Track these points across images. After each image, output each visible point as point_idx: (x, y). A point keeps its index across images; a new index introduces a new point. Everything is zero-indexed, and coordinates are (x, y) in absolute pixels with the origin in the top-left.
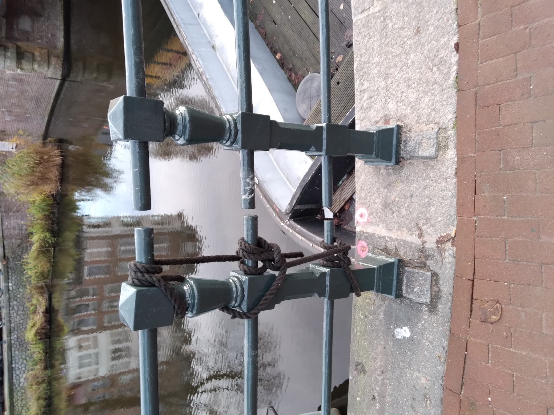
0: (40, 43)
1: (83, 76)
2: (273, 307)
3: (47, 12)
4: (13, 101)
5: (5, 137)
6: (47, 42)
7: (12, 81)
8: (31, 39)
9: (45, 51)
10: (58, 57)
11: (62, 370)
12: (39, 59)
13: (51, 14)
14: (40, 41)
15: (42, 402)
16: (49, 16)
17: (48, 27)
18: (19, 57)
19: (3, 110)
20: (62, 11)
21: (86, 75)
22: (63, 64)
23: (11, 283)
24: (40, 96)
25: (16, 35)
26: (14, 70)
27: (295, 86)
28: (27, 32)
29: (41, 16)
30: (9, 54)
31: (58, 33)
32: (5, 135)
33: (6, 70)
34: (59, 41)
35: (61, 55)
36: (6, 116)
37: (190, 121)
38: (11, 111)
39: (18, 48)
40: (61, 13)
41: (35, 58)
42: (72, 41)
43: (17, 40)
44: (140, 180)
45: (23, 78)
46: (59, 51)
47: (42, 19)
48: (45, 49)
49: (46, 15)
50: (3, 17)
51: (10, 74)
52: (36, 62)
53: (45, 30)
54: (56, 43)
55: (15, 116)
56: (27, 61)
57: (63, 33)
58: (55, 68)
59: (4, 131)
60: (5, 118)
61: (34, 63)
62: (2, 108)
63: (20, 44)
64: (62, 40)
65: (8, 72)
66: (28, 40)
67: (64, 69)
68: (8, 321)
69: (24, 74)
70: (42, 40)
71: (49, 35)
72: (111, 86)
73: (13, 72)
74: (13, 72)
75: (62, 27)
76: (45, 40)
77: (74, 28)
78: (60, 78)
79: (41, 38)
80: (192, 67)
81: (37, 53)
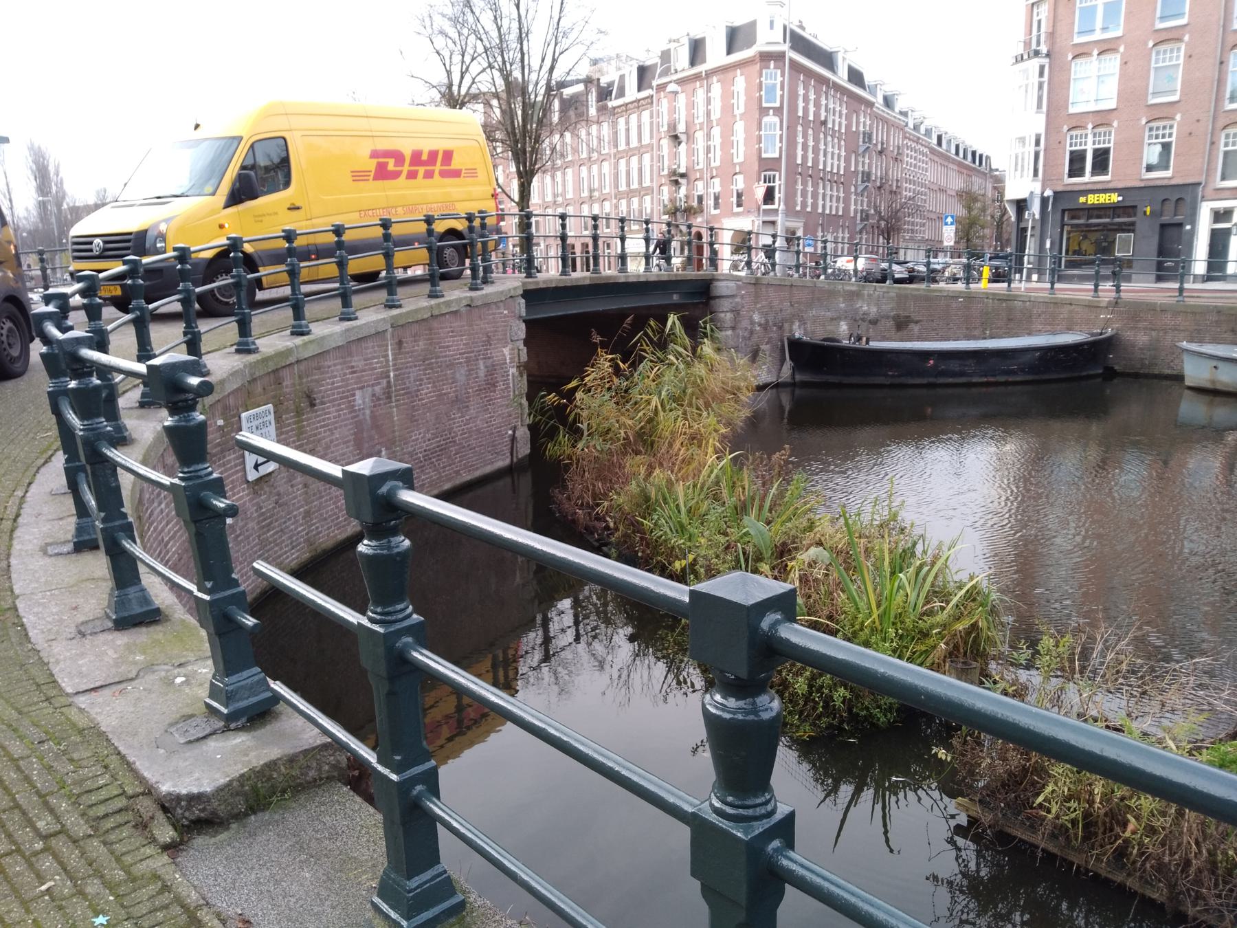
2: (694, 874)
4: (427, 390)
5: (289, 418)
7: (486, 367)
19: (392, 374)
23: (752, 323)
32: (299, 413)
33: (510, 346)
36: (370, 389)
37: (789, 412)
38: (389, 397)
44: (488, 733)
45: (501, 386)
51: (504, 355)
55: (373, 417)
59: (312, 405)
60: (362, 388)
62: (395, 370)
65: (506, 351)
68: (214, 813)
69: (508, 384)
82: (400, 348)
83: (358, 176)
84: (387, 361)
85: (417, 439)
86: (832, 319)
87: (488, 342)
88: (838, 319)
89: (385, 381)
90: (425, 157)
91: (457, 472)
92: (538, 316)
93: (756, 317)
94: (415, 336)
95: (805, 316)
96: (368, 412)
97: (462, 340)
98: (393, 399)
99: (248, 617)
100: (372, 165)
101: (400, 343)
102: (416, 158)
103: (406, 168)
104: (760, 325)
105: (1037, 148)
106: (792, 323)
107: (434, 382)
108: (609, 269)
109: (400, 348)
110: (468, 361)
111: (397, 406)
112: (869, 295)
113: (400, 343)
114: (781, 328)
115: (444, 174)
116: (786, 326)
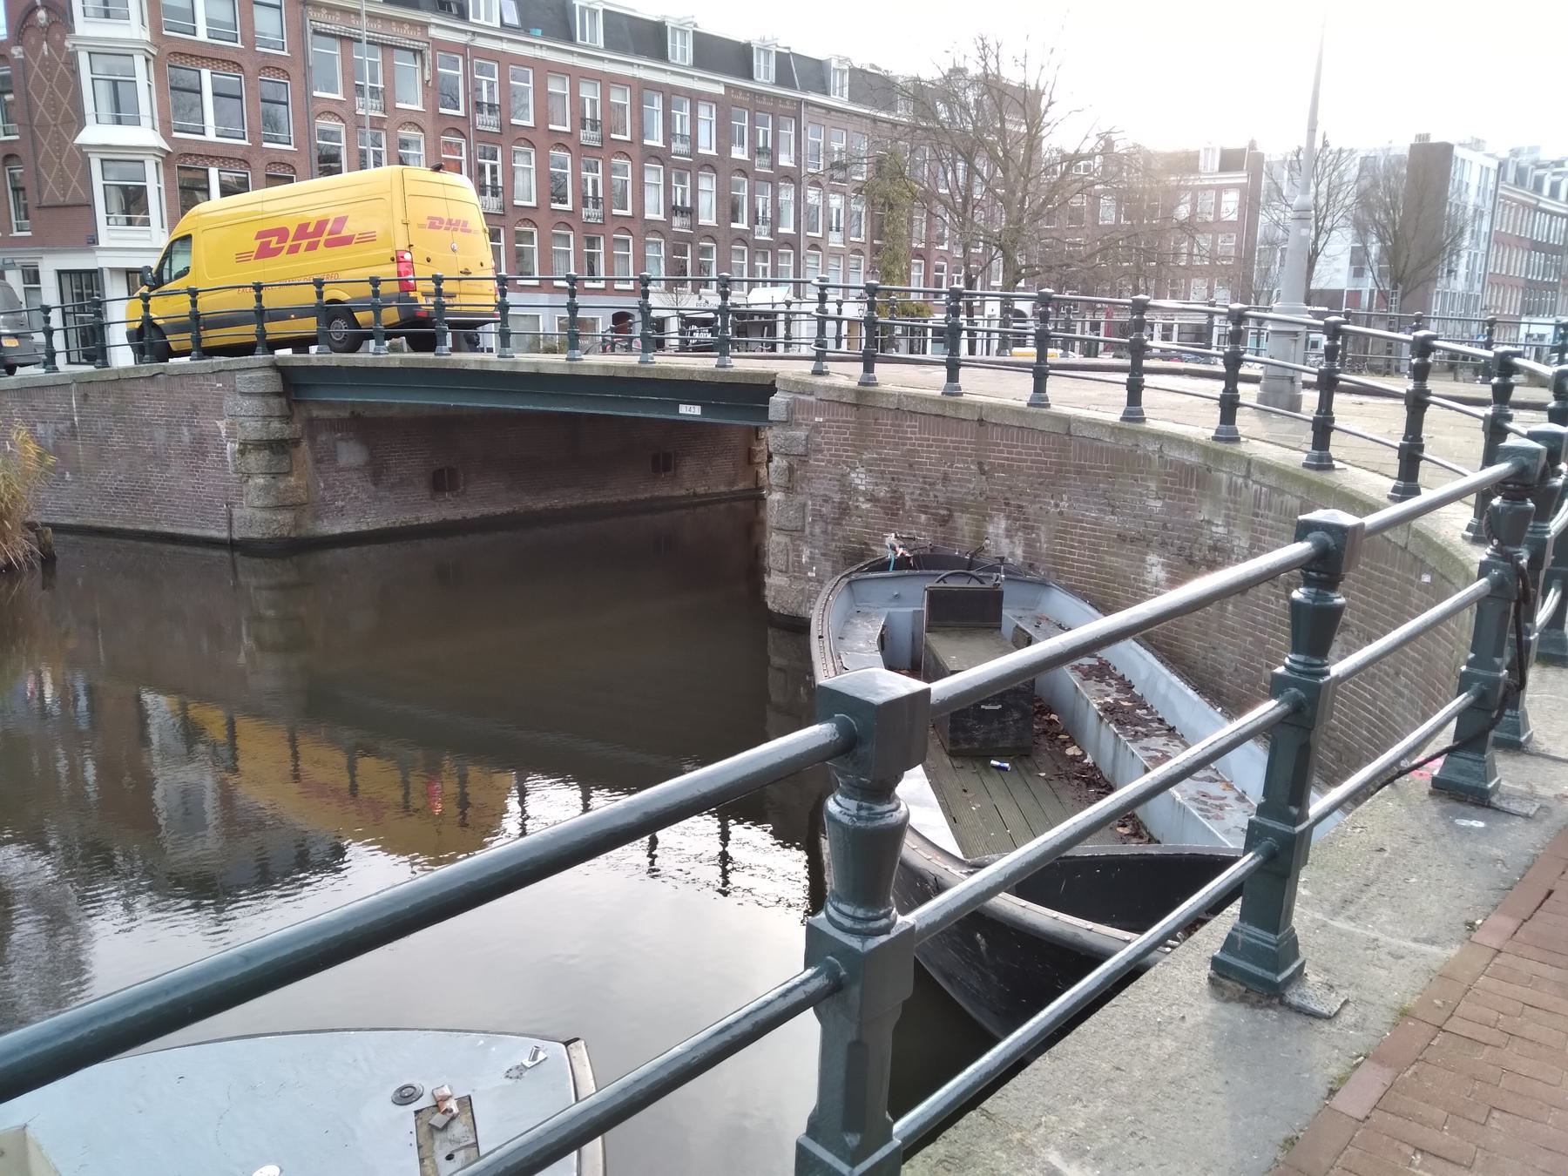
0: (319, 486)
1: (258, 588)
3: (388, 493)
6: (323, 499)
8: (322, 467)
9: (304, 497)
10: (297, 526)
11: (86, 951)
12: (282, 485)
13: (385, 504)
14: (322, 485)
15: (141, 902)
16: (381, 500)
17: (357, 498)
18: (274, 445)
19: (76, 419)
20: (397, 525)
21: (265, 593)
22: (281, 538)
23: (847, 489)
24: (151, 499)
25: (322, 438)
26: (231, 435)
27: (25, 1126)
28: (333, 457)
29: (376, 485)
30: (275, 425)
31: (351, 521)
34: (332, 525)
35: (303, 532)
36: (53, 426)
39: (296, 443)
40: (394, 523)
41: (281, 477)
42: (339, 551)
43: (312, 439)
45: (213, 456)
46: (309, 527)
47: (373, 488)
48: (308, 497)
49: (381, 494)
50: (353, 413)
52: (273, 481)
53: (348, 494)
54: (327, 517)
56: (270, 461)
57: (352, 530)
58: (268, 522)
61: (268, 477)
63: (304, 444)
64: (338, 531)
66: (318, 461)
67: (270, 541)
70: (325, 489)
71: (340, 503)
72: (242, 659)
73: (224, 434)
74: (224, 434)
75: (364, 528)
76: (328, 495)
77: (372, 552)
78: (236, 536)
79: (328, 487)
80: (972, 873)
81: (292, 480)
82: (85, 400)
83: (242, 257)
84: (71, 408)
85: (107, 476)
86: (1122, 538)
87: (195, 409)
88: (1142, 542)
89: (68, 423)
90: (311, 229)
91: (157, 520)
92: (623, 414)
93: (860, 479)
94: (104, 394)
95: (1031, 509)
96: (50, 441)
97: (161, 404)
98: (79, 438)
99: (1254, 862)
100: (428, 222)
101: (85, 396)
102: (302, 231)
103: (444, 225)
104: (873, 499)
105: (681, 50)
106: (985, 518)
107: (126, 435)
108: (988, 354)
109: (85, 400)
110: (168, 424)
111: (82, 444)
112: (1234, 489)
113: (85, 396)
114: (945, 521)
115: (462, 230)
116: (963, 521)
